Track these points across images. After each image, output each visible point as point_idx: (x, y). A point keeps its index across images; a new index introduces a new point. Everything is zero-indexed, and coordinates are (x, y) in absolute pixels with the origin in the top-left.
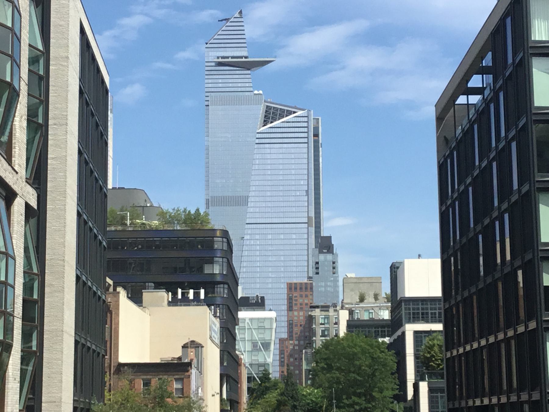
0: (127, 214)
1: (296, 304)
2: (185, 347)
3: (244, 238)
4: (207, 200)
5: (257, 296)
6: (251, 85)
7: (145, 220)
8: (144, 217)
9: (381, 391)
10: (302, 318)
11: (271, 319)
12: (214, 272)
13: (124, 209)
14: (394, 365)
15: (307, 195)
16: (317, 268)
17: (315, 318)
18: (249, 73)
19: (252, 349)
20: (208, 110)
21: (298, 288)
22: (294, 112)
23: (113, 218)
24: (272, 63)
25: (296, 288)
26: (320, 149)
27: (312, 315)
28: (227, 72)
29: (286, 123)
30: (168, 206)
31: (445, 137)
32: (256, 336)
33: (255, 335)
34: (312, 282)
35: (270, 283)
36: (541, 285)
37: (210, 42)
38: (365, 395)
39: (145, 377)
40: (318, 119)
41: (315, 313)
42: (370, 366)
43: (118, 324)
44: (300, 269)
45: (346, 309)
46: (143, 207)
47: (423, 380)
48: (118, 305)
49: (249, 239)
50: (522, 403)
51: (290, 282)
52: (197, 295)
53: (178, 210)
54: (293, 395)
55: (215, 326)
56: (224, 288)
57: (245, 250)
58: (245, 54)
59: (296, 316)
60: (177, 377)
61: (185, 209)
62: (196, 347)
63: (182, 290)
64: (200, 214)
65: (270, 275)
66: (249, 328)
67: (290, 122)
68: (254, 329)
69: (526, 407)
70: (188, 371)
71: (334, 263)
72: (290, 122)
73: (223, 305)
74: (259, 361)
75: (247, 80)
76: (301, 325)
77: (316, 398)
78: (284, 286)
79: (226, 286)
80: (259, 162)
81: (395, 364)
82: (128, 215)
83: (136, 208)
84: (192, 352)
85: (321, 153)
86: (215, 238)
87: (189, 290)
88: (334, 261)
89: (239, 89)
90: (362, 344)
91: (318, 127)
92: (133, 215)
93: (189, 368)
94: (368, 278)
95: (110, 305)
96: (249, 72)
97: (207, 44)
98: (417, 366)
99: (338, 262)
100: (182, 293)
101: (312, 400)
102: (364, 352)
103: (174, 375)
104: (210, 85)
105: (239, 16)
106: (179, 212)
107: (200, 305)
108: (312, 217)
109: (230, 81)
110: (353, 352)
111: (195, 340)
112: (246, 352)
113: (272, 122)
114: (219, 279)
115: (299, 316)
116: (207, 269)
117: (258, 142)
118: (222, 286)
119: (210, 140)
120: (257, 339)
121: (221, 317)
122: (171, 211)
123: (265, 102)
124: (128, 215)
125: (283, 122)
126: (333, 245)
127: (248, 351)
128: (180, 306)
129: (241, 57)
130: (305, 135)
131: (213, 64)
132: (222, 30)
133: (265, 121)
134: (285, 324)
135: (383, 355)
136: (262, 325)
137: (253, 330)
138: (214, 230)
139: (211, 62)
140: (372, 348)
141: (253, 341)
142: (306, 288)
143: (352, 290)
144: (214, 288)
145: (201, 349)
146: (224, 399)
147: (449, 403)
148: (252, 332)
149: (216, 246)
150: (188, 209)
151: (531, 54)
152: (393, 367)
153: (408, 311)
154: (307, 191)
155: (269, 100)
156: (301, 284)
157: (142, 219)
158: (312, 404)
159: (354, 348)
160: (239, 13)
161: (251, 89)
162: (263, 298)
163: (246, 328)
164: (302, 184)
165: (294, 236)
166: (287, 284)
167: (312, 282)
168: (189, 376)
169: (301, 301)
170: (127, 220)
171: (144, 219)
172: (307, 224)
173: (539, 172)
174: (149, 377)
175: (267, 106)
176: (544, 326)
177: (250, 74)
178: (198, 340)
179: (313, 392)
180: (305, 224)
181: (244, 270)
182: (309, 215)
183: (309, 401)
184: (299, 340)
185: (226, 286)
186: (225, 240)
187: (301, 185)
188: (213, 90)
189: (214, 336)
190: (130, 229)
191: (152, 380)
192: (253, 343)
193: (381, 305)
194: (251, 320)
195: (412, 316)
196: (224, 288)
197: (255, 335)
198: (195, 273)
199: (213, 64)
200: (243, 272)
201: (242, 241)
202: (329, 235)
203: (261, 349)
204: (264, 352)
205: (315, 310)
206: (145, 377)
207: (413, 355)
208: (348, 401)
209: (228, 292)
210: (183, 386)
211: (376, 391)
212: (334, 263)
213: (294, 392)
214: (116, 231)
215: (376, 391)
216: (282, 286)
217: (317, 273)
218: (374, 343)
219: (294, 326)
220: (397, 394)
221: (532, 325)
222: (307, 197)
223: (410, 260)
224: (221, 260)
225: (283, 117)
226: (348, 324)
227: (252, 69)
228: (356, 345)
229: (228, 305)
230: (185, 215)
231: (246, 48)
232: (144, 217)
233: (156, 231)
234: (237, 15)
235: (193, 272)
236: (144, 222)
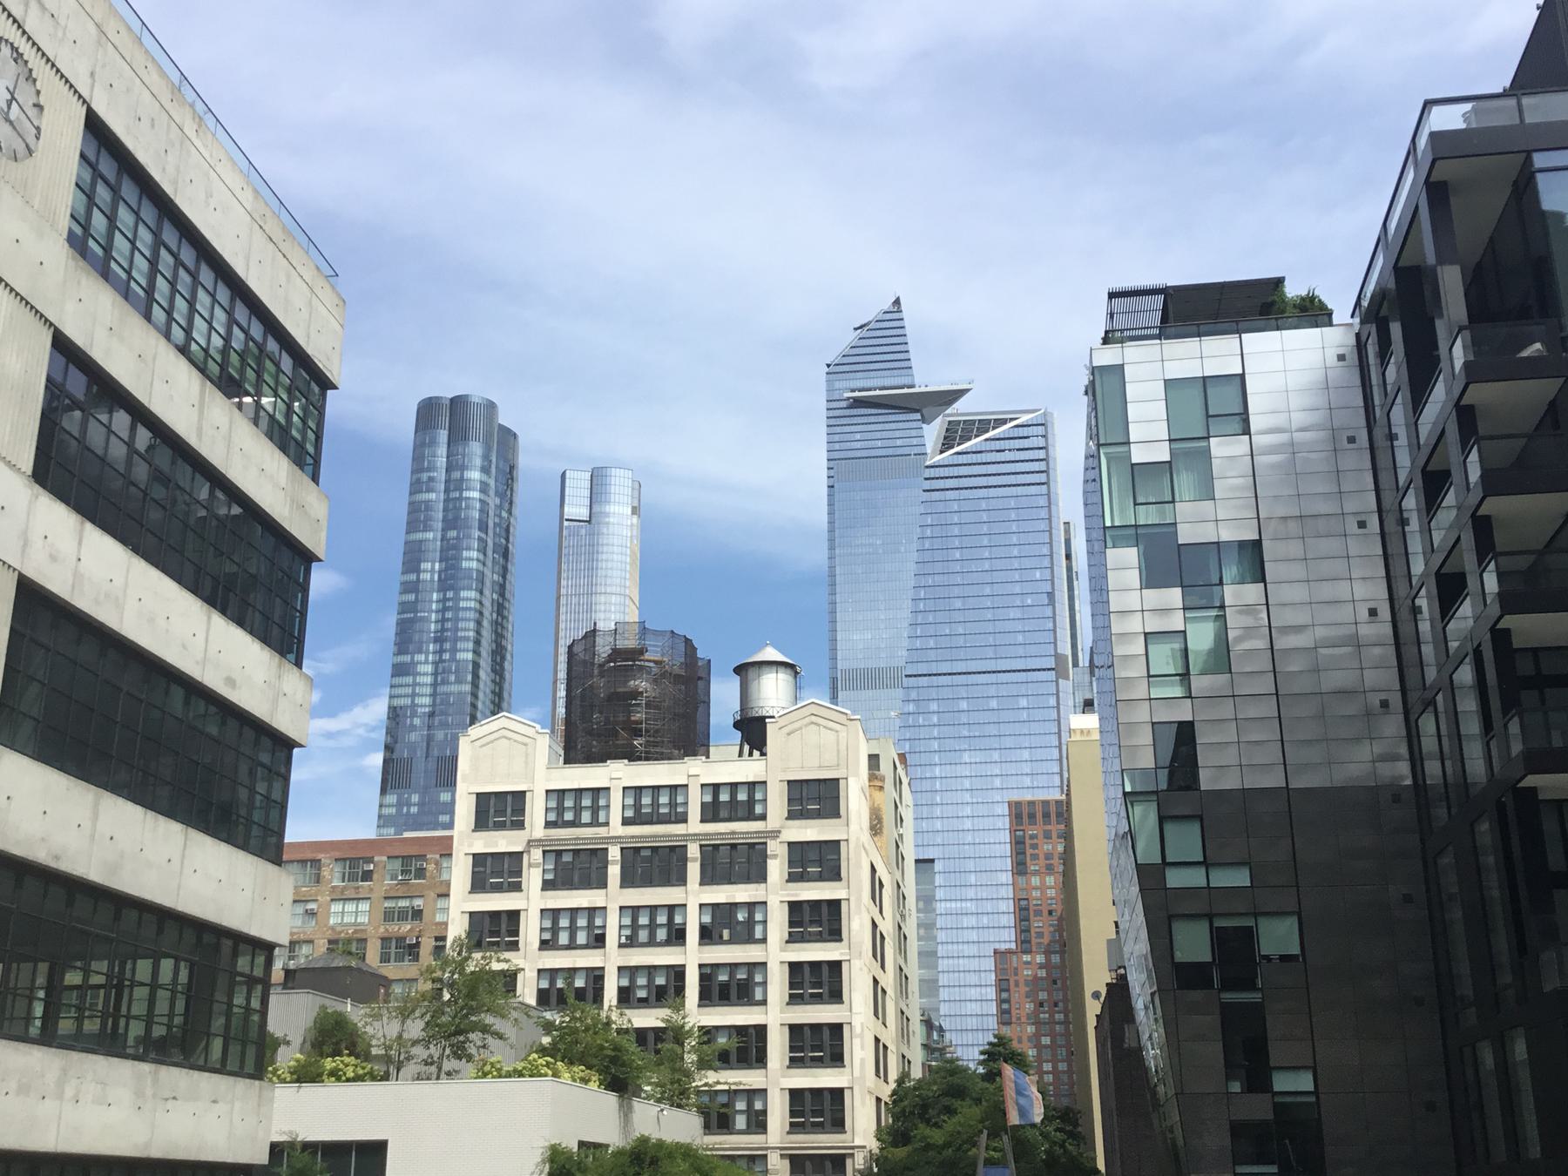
1: (1035, 857)
10: (1051, 893)
21: (1039, 816)
25: (1032, 816)
28: (872, 419)
59: (1035, 888)
65: (967, 797)
76: (1050, 913)
108: (1067, 656)
115: (1043, 888)
125: (986, 440)
134: (1008, 906)
156: (1046, 803)
169: (1047, 847)
172: (1054, 672)
175: (950, 422)
182: (1059, 651)
184: (1048, 953)
219: (1032, 913)
225: (987, 431)
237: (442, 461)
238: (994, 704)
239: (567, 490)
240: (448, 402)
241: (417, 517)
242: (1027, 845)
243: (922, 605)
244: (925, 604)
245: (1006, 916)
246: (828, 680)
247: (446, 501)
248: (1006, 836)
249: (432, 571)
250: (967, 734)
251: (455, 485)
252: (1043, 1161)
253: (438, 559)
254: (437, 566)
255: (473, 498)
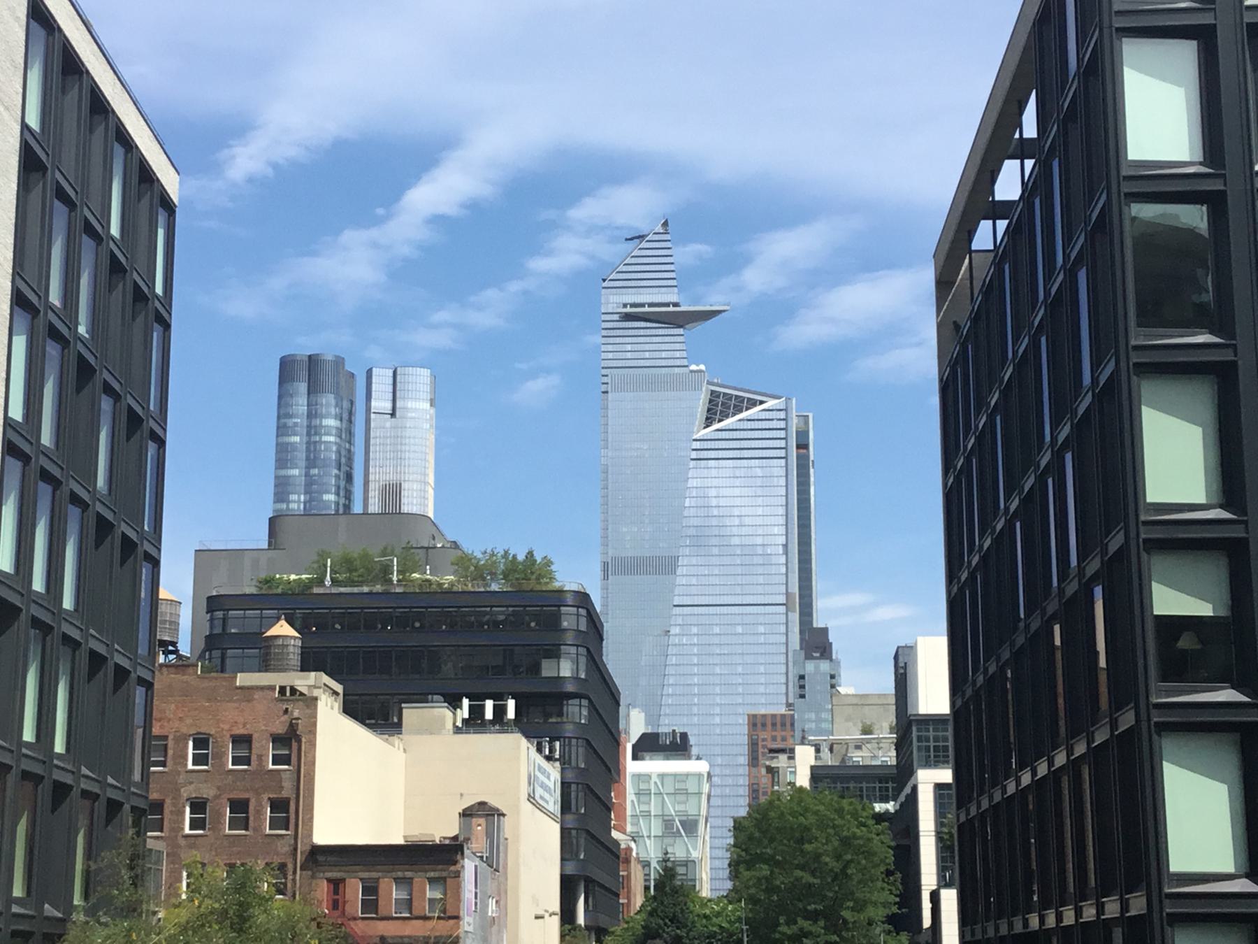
0: (392, 561)
2: (467, 814)
3: (669, 631)
4: (605, 566)
5: (674, 731)
6: (684, 354)
7: (431, 574)
8: (428, 567)
9: (860, 907)
11: (700, 775)
12: (561, 675)
13: (389, 551)
14: (888, 853)
15: (786, 553)
16: (802, 687)
17: (778, 772)
18: (682, 333)
19: (663, 833)
20: (607, 399)
22: (762, 402)
23: (367, 569)
24: (723, 314)
25: (764, 725)
26: (812, 471)
27: (773, 766)
28: (642, 332)
29: (746, 422)
30: (476, 546)
31: (955, 322)
32: (671, 808)
33: (670, 806)
34: (792, 712)
35: (718, 715)
36: (1147, 614)
37: (611, 277)
38: (826, 918)
39: (366, 875)
40: (808, 416)
41: (779, 762)
42: (838, 857)
43: (313, 763)
44: (771, 689)
45: (810, 744)
46: (427, 548)
47: (948, 885)
48: (315, 724)
49: (679, 635)
50: (1108, 925)
51: (753, 712)
52: (500, 711)
53: (493, 555)
54: (674, 916)
55: (548, 778)
56: (580, 706)
57: (672, 655)
58: (674, 299)
60: (432, 874)
61: (506, 552)
62: (488, 815)
63: (470, 701)
64: (536, 561)
66: (658, 792)
67: (753, 420)
68: (667, 794)
69: (1118, 935)
70: (455, 863)
71: (832, 677)
72: (753, 420)
73: (577, 738)
74: (677, 856)
75: (678, 346)
77: (730, 922)
78: (743, 720)
79: (585, 702)
80: (697, 493)
81: (890, 851)
82: (395, 563)
83: (412, 551)
84: (479, 825)
85: (812, 479)
86: (562, 608)
87: (484, 701)
88: (832, 673)
89: (664, 363)
90: (822, 808)
91: (807, 432)
92: (405, 564)
93: (459, 857)
94: (879, 696)
95: (297, 724)
96: (681, 331)
97: (604, 280)
98: (942, 857)
99: (840, 676)
100: (470, 706)
101: (721, 927)
102: (823, 824)
103: (426, 871)
104: (610, 356)
105: (662, 231)
106: (495, 558)
107: (506, 732)
109: (647, 347)
110: (800, 824)
111: (486, 801)
112: (652, 838)
113: (720, 421)
114: (570, 688)
116: (547, 669)
117: (695, 457)
118: (576, 701)
119: (610, 454)
120: (673, 814)
121: (562, 759)
122: (480, 556)
123: (709, 383)
124: (395, 563)
125: (740, 420)
126: (831, 643)
127: (655, 837)
128: (466, 733)
129: (667, 305)
130: (782, 444)
131: (616, 317)
132: (633, 257)
133: (707, 419)
135: (862, 831)
136: (681, 786)
137: (665, 796)
138: (561, 592)
139: (612, 313)
140: (842, 817)
141: (666, 818)
142: (783, 725)
143: (848, 719)
144: (562, 705)
145: (499, 821)
146: (580, 925)
147: (964, 928)
148: (663, 798)
149: (565, 624)
150: (512, 552)
151: (1117, 29)
152: (886, 857)
153: (924, 744)
154: (786, 546)
155: (716, 381)
156: (774, 716)
157: (425, 573)
158: (721, 934)
159: (801, 815)
160: (664, 224)
161: (685, 362)
162: (684, 736)
163: (653, 792)
164: (776, 533)
165: (761, 629)
166: (748, 715)
167: (792, 712)
168: (459, 872)
170: (392, 574)
171: (428, 572)
172: (784, 607)
173: (1139, 325)
174: (374, 875)
175: (713, 392)
176: (1155, 719)
177: (682, 335)
178: (494, 802)
179: (724, 909)
180: (781, 607)
181: (670, 691)
182: (789, 591)
183: (714, 929)
185: (585, 702)
186: (583, 612)
187: (775, 535)
188: (615, 364)
189: (541, 797)
190: (399, 590)
191: (381, 880)
192: (664, 821)
193: (881, 736)
194: (662, 776)
195: (932, 754)
196: (580, 706)
197: (670, 806)
198: (523, 675)
199: (616, 317)
200: (668, 695)
201: (667, 637)
202: (824, 626)
203: (680, 833)
204: (686, 838)
205: (777, 757)
206: (366, 875)
207: (933, 833)
208: (789, 928)
209: (589, 713)
210: (411, 894)
211: (848, 908)
212: (832, 677)
213: (678, 909)
214: (370, 593)
215: (848, 908)
216: (741, 721)
217: (802, 696)
218: (847, 808)
220: (894, 914)
221: (1127, 720)
222: (784, 556)
223: (927, 638)
224: (573, 650)
225: (741, 411)
226: (812, 774)
227: (687, 326)
228: (806, 810)
229: (587, 740)
230: (505, 564)
231: (676, 289)
232: (428, 567)
233: (449, 592)
234: (659, 229)
235: (520, 674)
236: (429, 577)
237: (303, 409)
238: (739, 629)
239: (374, 387)
240: (307, 359)
241: (283, 456)
242: (760, 746)
243: (688, 550)
244: (690, 550)
245: (742, 767)
246: (599, 563)
247: (308, 443)
248: (745, 740)
249: (299, 501)
250: (718, 652)
251: (312, 430)
252: (275, 576)
253: (303, 491)
254: (302, 498)
255: (330, 442)
